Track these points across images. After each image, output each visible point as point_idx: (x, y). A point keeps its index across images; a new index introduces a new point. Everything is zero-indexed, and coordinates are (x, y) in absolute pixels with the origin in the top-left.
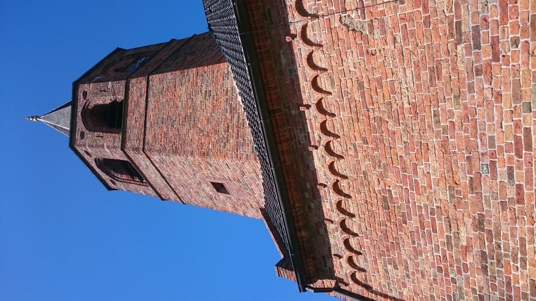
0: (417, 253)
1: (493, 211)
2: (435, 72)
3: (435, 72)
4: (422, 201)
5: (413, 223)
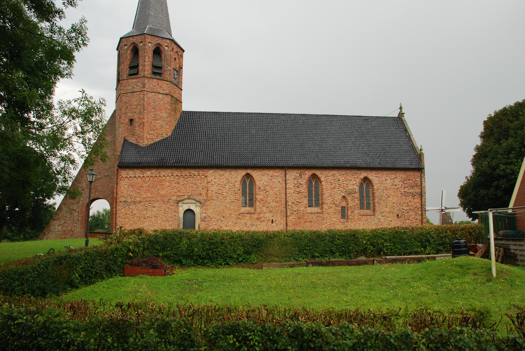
0: (132, 191)
1: (143, 204)
2: (164, 196)
3: (164, 196)
4: (143, 192)
5: (138, 191)
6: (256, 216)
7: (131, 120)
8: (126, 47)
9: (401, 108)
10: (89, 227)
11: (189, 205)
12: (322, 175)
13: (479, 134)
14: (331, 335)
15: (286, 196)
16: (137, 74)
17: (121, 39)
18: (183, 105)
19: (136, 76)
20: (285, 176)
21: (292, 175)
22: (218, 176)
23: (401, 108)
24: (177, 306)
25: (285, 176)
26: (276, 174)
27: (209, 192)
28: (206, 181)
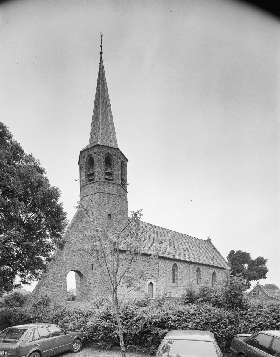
6: (178, 288)
7: (109, 215)
8: (85, 159)
9: (209, 237)
10: (172, 341)
11: (151, 280)
12: (202, 268)
13: (60, 189)
14: (145, 323)
15: (189, 278)
16: (93, 179)
17: (81, 152)
18: (251, 256)
19: (93, 182)
20: (189, 267)
21: (192, 266)
22: (163, 264)
23: (209, 237)
24: (80, 318)
25: (189, 267)
26: (186, 266)
27: (160, 272)
28: (158, 266)
